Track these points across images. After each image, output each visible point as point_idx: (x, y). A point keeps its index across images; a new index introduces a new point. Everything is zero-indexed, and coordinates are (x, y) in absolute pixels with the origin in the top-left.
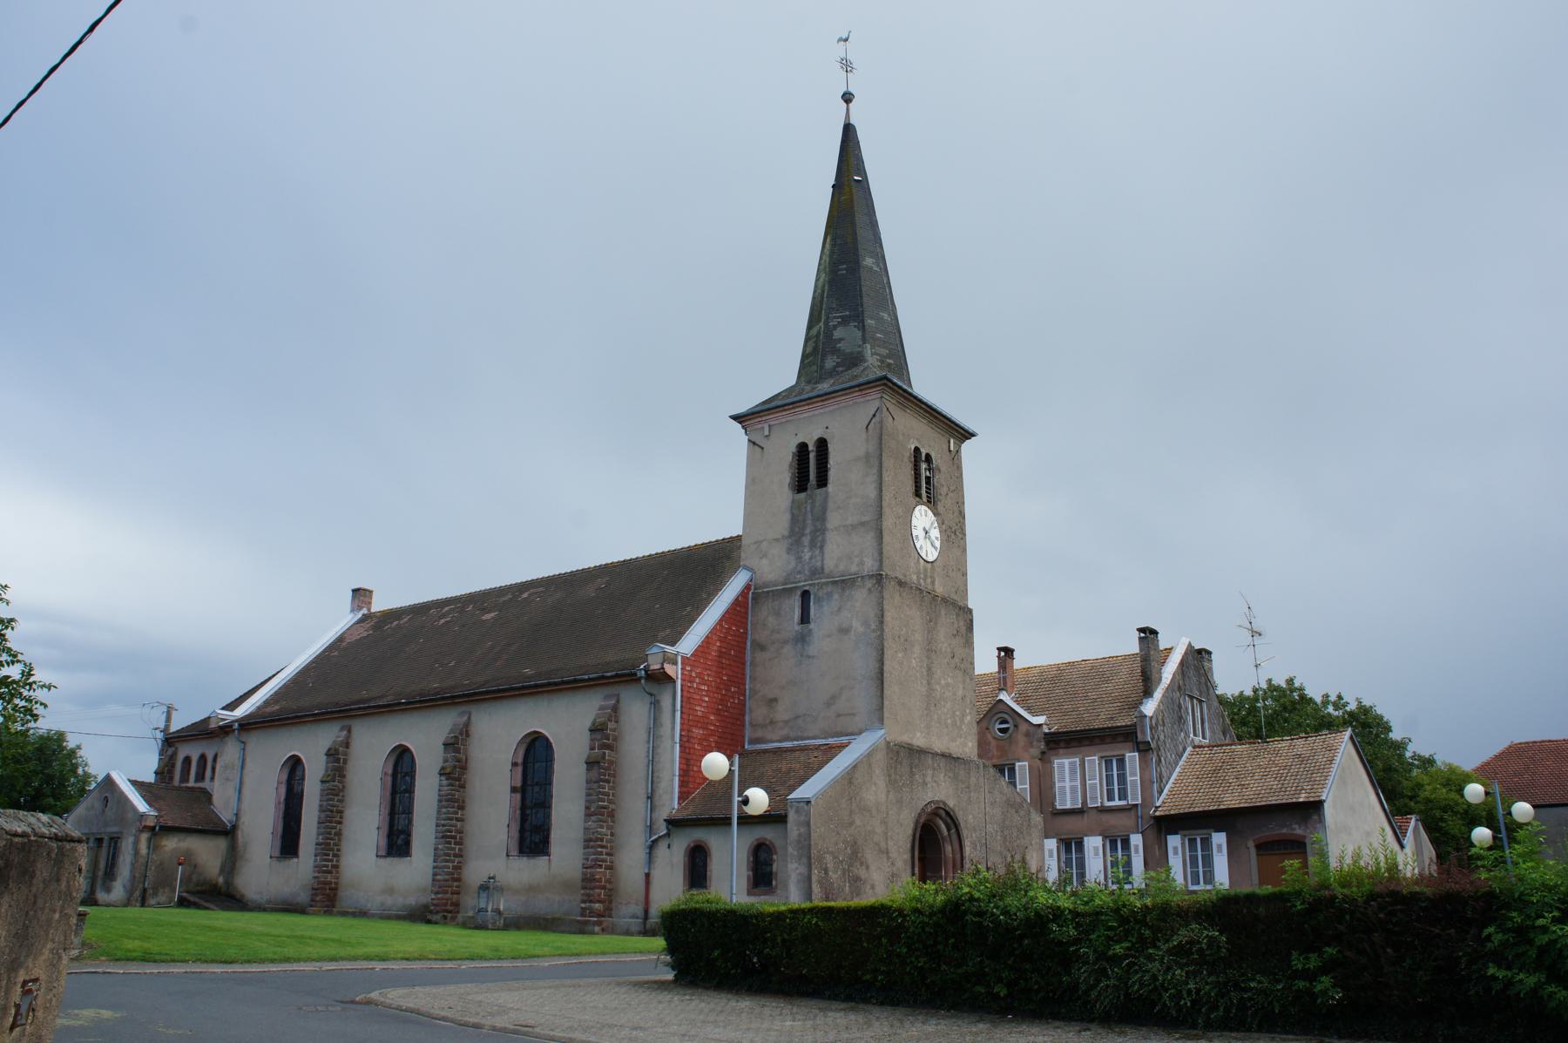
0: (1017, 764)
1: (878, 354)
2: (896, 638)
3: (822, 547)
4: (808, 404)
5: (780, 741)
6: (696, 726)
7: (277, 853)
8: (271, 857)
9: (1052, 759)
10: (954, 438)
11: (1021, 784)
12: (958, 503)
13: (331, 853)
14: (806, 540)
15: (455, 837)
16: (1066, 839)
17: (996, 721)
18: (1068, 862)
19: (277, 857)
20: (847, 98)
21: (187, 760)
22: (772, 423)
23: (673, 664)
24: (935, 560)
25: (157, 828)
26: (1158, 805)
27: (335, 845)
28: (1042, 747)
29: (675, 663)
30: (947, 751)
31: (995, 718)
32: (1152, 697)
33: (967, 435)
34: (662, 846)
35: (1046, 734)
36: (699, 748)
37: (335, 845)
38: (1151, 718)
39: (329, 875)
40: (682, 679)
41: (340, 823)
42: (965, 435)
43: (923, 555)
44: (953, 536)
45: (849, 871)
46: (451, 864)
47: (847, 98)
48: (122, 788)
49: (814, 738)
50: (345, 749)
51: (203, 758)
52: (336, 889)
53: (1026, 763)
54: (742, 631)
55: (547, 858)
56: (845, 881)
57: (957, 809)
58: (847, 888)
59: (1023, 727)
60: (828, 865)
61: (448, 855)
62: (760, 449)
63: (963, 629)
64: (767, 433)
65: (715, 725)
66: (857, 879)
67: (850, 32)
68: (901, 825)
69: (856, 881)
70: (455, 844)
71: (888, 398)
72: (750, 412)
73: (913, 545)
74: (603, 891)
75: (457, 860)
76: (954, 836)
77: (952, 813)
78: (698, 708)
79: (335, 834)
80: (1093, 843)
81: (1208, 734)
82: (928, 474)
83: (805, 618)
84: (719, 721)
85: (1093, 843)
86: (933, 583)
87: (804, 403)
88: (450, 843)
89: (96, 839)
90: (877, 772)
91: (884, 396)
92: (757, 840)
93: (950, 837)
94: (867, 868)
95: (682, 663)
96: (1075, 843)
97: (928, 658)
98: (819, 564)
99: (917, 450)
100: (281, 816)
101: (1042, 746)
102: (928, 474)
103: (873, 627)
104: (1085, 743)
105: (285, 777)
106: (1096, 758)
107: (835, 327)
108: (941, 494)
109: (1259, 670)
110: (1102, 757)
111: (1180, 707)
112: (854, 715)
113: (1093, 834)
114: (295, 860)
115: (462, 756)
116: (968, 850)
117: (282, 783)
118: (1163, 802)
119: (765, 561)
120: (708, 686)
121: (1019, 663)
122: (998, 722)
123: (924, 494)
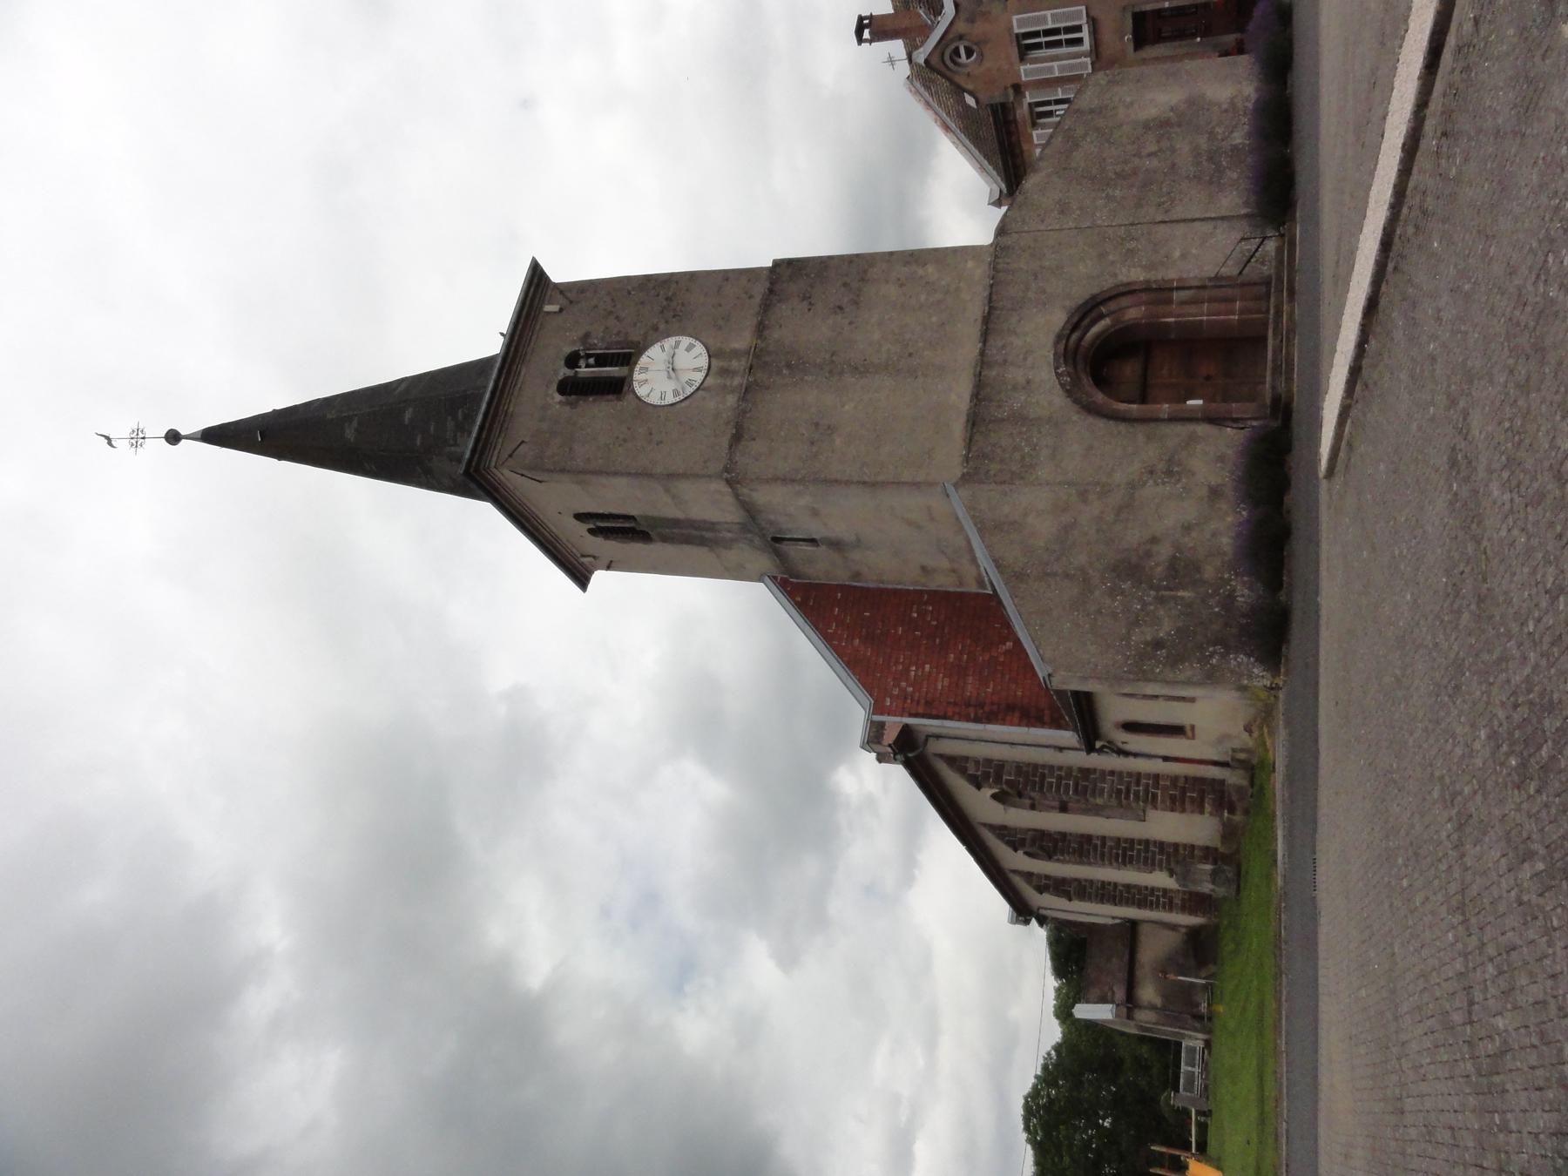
0: (1017, 31)
10: (542, 303)
11: (1046, 23)
14: (708, 535)
15: (1125, 849)
20: (173, 437)
27: (1140, 893)
29: (882, 725)
31: (948, 62)
36: (991, 686)
37: (1140, 893)
41: (1116, 885)
47: (173, 437)
53: (1015, 18)
56: (1175, 598)
57: (1068, 303)
59: (961, 27)
60: (1149, 638)
61: (1146, 858)
65: (961, 653)
66: (1173, 566)
69: (1182, 570)
71: (494, 459)
73: (687, 402)
74: (1188, 794)
75: (1152, 848)
76: (1113, 306)
77: (1075, 319)
79: (1128, 892)
82: (591, 361)
86: (735, 354)
90: (1006, 509)
93: (1114, 312)
94: (1154, 540)
95: (882, 714)
115: (1029, 836)
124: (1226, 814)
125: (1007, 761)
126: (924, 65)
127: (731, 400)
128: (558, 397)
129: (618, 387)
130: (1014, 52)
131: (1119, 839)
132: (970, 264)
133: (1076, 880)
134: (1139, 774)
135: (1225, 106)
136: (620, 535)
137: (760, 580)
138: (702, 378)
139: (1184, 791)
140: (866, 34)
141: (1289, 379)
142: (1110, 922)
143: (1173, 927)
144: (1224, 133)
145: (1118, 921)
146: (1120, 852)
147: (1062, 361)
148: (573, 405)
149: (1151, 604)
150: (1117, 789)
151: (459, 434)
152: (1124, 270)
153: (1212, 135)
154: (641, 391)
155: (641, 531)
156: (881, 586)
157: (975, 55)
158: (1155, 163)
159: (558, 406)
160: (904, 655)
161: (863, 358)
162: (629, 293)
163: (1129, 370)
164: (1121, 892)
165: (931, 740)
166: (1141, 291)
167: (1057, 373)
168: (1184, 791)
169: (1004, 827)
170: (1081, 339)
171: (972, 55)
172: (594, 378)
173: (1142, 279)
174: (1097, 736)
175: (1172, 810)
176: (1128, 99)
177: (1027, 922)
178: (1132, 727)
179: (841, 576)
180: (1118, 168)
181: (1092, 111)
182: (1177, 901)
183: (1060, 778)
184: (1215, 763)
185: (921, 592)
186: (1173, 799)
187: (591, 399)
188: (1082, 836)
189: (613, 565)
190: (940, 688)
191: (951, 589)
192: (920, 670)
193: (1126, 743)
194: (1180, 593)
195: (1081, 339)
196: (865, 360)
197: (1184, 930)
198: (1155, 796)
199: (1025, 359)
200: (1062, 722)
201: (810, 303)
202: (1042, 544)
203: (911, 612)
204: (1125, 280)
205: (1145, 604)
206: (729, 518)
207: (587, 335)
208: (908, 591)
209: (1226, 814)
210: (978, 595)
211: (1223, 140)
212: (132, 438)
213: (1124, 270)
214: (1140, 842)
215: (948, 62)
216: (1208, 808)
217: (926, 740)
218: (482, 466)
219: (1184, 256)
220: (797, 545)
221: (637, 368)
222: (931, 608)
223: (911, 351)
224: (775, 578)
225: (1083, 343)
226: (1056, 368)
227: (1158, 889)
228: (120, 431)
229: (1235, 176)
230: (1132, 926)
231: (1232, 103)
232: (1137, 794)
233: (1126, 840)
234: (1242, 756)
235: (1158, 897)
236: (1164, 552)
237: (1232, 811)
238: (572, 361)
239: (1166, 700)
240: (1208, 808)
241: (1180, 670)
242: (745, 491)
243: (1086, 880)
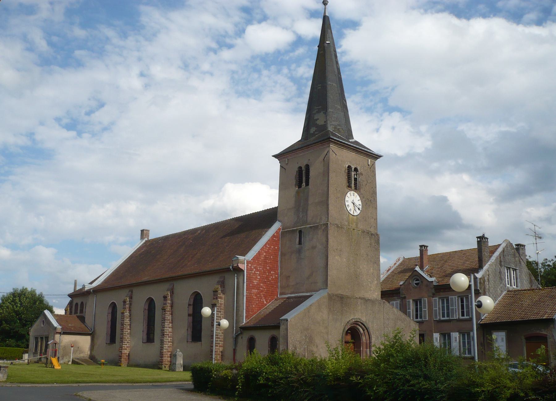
1: (332, 125)
2: (336, 250)
3: (307, 212)
4: (302, 150)
5: (291, 294)
6: (254, 289)
7: (109, 342)
8: (106, 343)
13: (126, 341)
16: (444, 333)
17: (414, 279)
18: (445, 343)
19: (191, 342)
21: (77, 304)
22: (288, 158)
23: (243, 264)
25: (62, 333)
26: (482, 318)
28: (433, 292)
31: (414, 278)
32: (483, 269)
34: (240, 337)
35: (434, 286)
38: (480, 279)
39: (126, 350)
40: (246, 270)
43: (352, 213)
46: (167, 346)
48: (48, 317)
49: (303, 292)
51: (82, 303)
54: (276, 248)
55: (200, 342)
62: (284, 170)
64: (287, 163)
70: (168, 337)
72: (282, 153)
76: (366, 333)
78: (255, 281)
80: (455, 335)
81: (519, 285)
82: (356, 176)
83: (300, 243)
84: (265, 286)
85: (455, 335)
87: (300, 150)
89: (41, 337)
92: (272, 335)
95: (247, 263)
96: (448, 335)
99: (349, 167)
100: (109, 327)
101: (433, 291)
102: (356, 176)
104: (442, 291)
105: (110, 311)
106: (437, 298)
108: (362, 185)
109: (538, 255)
110: (459, 296)
111: (500, 272)
113: (454, 331)
114: (115, 344)
116: (373, 340)
117: (109, 313)
118: (485, 317)
120: (260, 272)
121: (431, 252)
122: (415, 280)
123: (353, 185)
126: (415, 270)
128: (347, 166)
129: (349, 186)
130: (416, 298)
146: (168, 333)
151: (333, 126)
152: (374, 336)
157: (416, 286)
159: (345, 166)
162: (372, 188)
163: (349, 338)
166: (370, 341)
171: (416, 285)
193: (242, 338)
203: (273, 271)
204: (372, 336)
207: (362, 174)
215: (414, 278)
221: (354, 192)
225: (358, 326)
238: (356, 170)
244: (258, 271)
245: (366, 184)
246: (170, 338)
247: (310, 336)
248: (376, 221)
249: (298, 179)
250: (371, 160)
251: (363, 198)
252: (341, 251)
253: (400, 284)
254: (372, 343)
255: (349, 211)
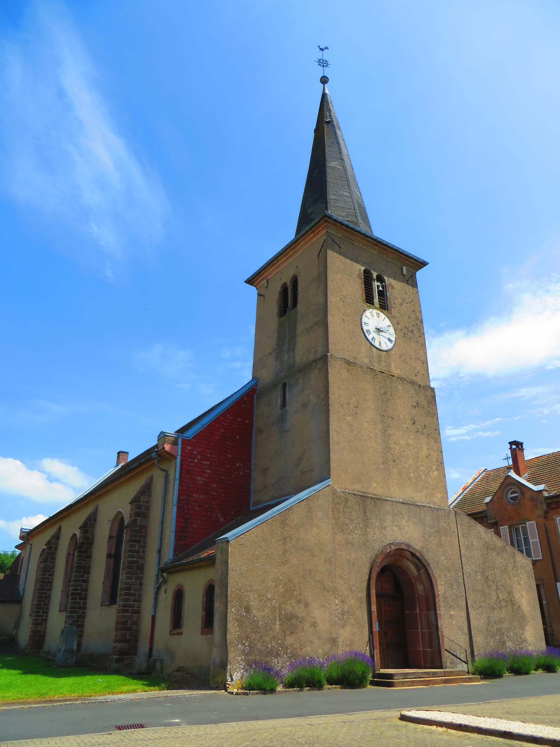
0: (527, 523)
2: (345, 405)
9: (554, 517)
10: (406, 266)
11: (532, 539)
12: (414, 311)
14: (285, 348)
15: (80, 594)
20: (324, 80)
24: (389, 350)
27: (44, 605)
30: (412, 500)
33: (421, 265)
35: (547, 498)
37: (44, 605)
41: (50, 590)
42: (421, 264)
44: (410, 334)
45: (280, 609)
47: (324, 80)
50: (56, 541)
52: (44, 636)
53: (534, 522)
57: (425, 551)
58: (277, 626)
61: (75, 608)
63: (424, 403)
66: (292, 617)
67: (327, 48)
68: (354, 565)
75: (81, 611)
77: (418, 554)
86: (389, 365)
88: (75, 599)
90: (320, 515)
91: (329, 231)
94: (307, 605)
95: (182, 444)
97: (383, 422)
98: (292, 362)
101: (544, 507)
103: (322, 397)
107: (309, 207)
112: (312, 470)
119: (264, 370)
121: (529, 454)
124: (116, 657)
125: (148, 520)
127: (366, 361)
129: (369, 300)
131: (87, 590)
132: (439, 495)
133: (54, 566)
134: (140, 601)
135: (522, 637)
136: (282, 300)
137: (254, 378)
138: (376, 346)
139: (130, 629)
140: (514, 447)
141: (403, 684)
142: (21, 588)
143: (17, 626)
144: (511, 637)
145: (21, 593)
147: (397, 547)
148: (359, 276)
149: (271, 604)
150: (132, 588)
153: (509, 629)
154: (368, 313)
155: (286, 311)
156: (253, 446)
158: (494, 598)
160: (215, 458)
161: (391, 434)
164: (46, 593)
165: (163, 473)
167: (391, 544)
168: (130, 629)
169: (95, 520)
170: (407, 559)
172: (372, 289)
173: (439, 593)
174: (170, 573)
175: (117, 623)
176: (522, 582)
177: (21, 538)
178: (179, 596)
179: (258, 422)
180: (490, 578)
181: (515, 562)
182: (39, 628)
183: (138, 552)
184: (151, 649)
185: (250, 468)
186: (125, 623)
187: (363, 286)
188: (89, 568)
189: (262, 297)
190: (197, 478)
191: (252, 486)
192: (208, 467)
193: (165, 592)
194: (278, 623)
195: (407, 559)
196: (390, 435)
197: (14, 632)
198: (127, 611)
199: (396, 526)
200: (178, 553)
201: (415, 407)
202: (301, 536)
205: (270, 600)
206: (298, 359)
208: (250, 461)
209: (116, 657)
210: (249, 501)
211: (507, 636)
212: (323, 61)
213: (442, 582)
214: (85, 603)
216: (119, 645)
217: (163, 470)
218: (328, 224)
219: (451, 616)
220: (281, 397)
222: (241, 474)
223: (396, 461)
224: (256, 386)
226: (393, 544)
227: (47, 616)
228: (326, 56)
229: (492, 644)
230: (18, 600)
231: (525, 640)
232: (128, 600)
233: (86, 595)
234: (158, 665)
235: (42, 616)
236: (300, 611)
237: (118, 661)
239: (152, 616)
240: (119, 645)
241: (234, 624)
242: (319, 366)
243: (53, 572)
244: (207, 461)
245: (402, 304)
246: (82, 601)
247: (286, 580)
248: (425, 365)
249: (282, 303)
250: (408, 269)
251: (398, 324)
252: (357, 407)
253: (485, 502)
254: (439, 597)
255: (370, 340)
